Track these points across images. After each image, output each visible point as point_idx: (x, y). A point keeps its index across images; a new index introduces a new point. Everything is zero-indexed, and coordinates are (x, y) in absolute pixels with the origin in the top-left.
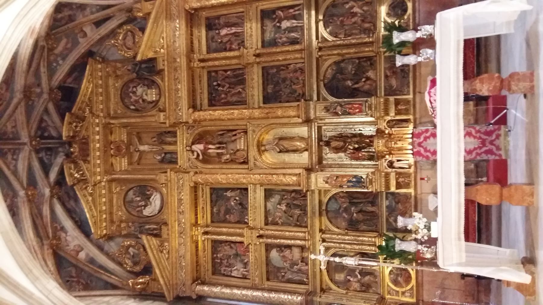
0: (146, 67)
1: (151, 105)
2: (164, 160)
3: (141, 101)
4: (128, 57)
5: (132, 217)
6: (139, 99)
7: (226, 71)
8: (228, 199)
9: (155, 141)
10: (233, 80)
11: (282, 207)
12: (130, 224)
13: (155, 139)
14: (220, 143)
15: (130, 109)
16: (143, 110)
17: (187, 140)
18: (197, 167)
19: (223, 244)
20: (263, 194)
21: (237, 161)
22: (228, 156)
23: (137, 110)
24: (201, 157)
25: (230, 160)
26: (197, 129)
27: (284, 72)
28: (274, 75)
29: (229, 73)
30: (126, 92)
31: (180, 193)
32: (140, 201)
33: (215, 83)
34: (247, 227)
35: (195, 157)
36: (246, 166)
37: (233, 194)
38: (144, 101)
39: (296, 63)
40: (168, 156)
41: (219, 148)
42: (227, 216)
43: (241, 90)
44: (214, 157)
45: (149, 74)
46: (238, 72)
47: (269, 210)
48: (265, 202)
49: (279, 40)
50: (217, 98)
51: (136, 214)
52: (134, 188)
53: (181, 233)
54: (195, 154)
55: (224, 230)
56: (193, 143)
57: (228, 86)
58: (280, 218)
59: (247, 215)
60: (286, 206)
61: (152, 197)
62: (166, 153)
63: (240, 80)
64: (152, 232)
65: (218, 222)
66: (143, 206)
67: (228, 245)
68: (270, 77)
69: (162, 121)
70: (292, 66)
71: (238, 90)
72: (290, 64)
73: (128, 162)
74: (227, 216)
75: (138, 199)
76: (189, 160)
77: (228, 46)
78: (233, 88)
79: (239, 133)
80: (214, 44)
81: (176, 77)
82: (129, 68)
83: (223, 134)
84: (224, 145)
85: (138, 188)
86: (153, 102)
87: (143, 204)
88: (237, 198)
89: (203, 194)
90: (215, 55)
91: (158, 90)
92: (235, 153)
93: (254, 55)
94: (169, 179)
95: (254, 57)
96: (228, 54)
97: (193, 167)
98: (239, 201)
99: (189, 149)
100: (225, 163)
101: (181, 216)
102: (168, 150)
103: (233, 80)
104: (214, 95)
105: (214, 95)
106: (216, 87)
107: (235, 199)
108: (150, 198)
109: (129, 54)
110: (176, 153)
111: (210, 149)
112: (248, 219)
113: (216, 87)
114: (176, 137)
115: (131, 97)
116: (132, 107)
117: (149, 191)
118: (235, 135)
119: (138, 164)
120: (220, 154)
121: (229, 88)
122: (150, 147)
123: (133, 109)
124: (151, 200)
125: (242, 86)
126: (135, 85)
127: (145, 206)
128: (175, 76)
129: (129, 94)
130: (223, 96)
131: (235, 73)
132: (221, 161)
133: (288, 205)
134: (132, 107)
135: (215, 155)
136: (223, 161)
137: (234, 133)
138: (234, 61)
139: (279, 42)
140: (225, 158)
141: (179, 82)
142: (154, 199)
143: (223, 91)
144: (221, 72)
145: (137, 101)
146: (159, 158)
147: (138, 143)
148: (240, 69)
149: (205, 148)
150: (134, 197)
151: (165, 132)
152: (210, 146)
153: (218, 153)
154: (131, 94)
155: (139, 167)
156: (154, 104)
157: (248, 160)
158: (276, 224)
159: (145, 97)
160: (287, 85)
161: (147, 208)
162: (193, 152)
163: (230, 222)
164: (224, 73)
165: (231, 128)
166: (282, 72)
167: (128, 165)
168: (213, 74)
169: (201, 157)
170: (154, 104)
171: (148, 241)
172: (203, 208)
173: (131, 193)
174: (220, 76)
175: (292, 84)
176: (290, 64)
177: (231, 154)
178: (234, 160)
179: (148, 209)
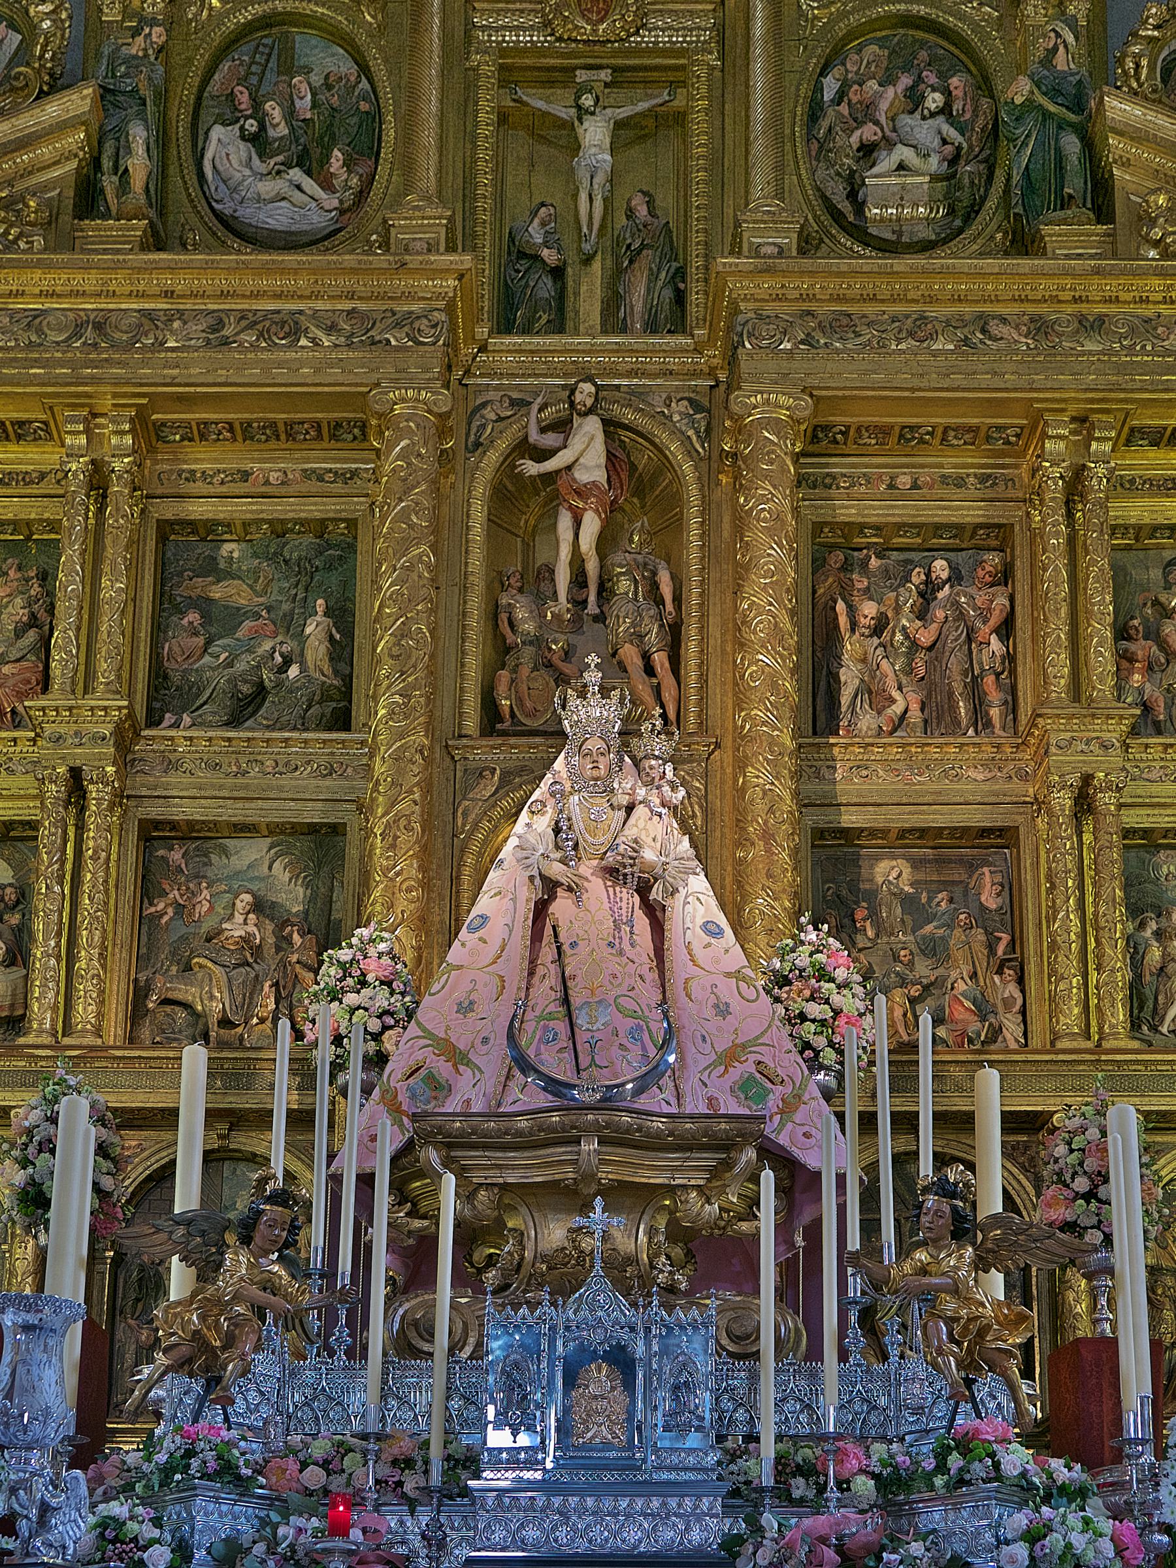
0: (1060, 160)
1: (838, 192)
2: (522, 265)
3: (869, 132)
4: (1120, 62)
5: (201, 61)
6: (877, 123)
7: (1006, 629)
8: (291, 625)
9: (630, 213)
10: (955, 664)
11: (239, 918)
12: (158, 34)
13: (643, 211)
14: (605, 590)
15: (823, 73)
16: (815, 146)
17: (632, 391)
18: (478, 445)
19: (35, 590)
20: (313, 815)
21: (504, 675)
22: (529, 627)
23: (815, 111)
24: (532, 468)
25: (510, 638)
26: (690, 452)
27: (981, 952)
28: (963, 894)
29: (995, 644)
30: (923, 55)
31: (331, 329)
32: (290, 113)
33: (941, 568)
34: (131, 716)
35: (534, 436)
36: (471, 724)
37: (317, 650)
38: (868, 151)
39: (1023, 1012)
40: (546, 287)
41: (579, 579)
42: (193, 617)
43: (898, 708)
44: (528, 548)
45: (1016, 178)
46: (994, 696)
47: (225, 851)
48: (274, 830)
49: (1153, 926)
50: (861, 583)
51: (214, 87)
52: (364, 84)
53: (99, 327)
54: (551, 440)
55: (112, 588)
56: (610, 426)
57: (925, 637)
58: (179, 908)
59: (75, 206)
60: (247, 939)
61: (309, 184)
62: (558, 273)
63: (954, 708)
64: (107, 164)
65: (162, 565)
66: (262, 127)
67: (33, 616)
68: (959, 874)
69: (752, 238)
70: (1012, 989)
71: (896, 694)
72: (1021, 981)
73: (518, 50)
74: (193, 617)
75: (304, 104)
76: (520, 404)
77: (1142, 648)
78: (909, 670)
79: (657, 691)
80: (1156, 574)
81: (996, 329)
82: (1061, 61)
83: (659, 601)
84: (592, 608)
85: (364, 106)
86: (859, 208)
87: (271, 133)
88: (294, 671)
89: (321, 479)
90: (1097, 566)
91: (926, 233)
92: (549, 665)
93: (1087, 779)
94: (413, 261)
95: (1073, 779)
96: (1100, 631)
97: (476, 424)
98: (279, 685)
99: (578, 397)
100: (494, 612)
101: (197, 328)
102: (577, 294)
103: (955, 664)
104: (874, 562)
105: (874, 562)
106: (918, 576)
107: (287, 662)
108: (309, 173)
109: (1138, 66)
110: (558, 326)
111: (577, 523)
112: (176, 725)
113: (918, 576)
114: (652, 327)
115: (887, 81)
116: (830, 86)
117: (348, 164)
118: (650, 670)
119: (503, 119)
120: (545, 586)
121: (914, 645)
122: (599, 179)
123: (818, 89)
124: (296, 174)
125: (915, 716)
126: (957, 107)
127: (258, 141)
128: (1004, 320)
129: (906, 69)
130: (869, 609)
131: (990, 680)
132: (503, 588)
133: (251, 949)
134: (830, 86)
135: (541, 559)
136: (504, 600)
137: (660, 659)
138: (1060, 665)
139: (1142, 926)
140: (520, 614)
141: (966, 341)
142: (297, 196)
143: (898, 609)
144: (1002, 601)
145: (865, 113)
146: (536, 234)
147: (623, 113)
148: (1012, 707)
149: (581, 492)
150: (317, 79)
151: (681, 273)
152: (591, 525)
153: (550, 571)
154: (905, 81)
155: (485, 116)
156: (845, 207)
157: (504, 734)
158: (148, 889)
159: (886, 162)
160: (911, 965)
161: (243, 149)
162: (563, 426)
163: (159, 630)
164: (995, 619)
165: (691, 649)
166: (979, 935)
167: (503, 52)
168: (993, 560)
169: (532, 468)
170: (845, 207)
171: (62, 127)
172: (245, 475)
173: (341, 64)
174: (981, 599)
175: (915, 991)
176: (1021, 981)
177: (538, 642)
178: (510, 660)
179: (244, 155)
